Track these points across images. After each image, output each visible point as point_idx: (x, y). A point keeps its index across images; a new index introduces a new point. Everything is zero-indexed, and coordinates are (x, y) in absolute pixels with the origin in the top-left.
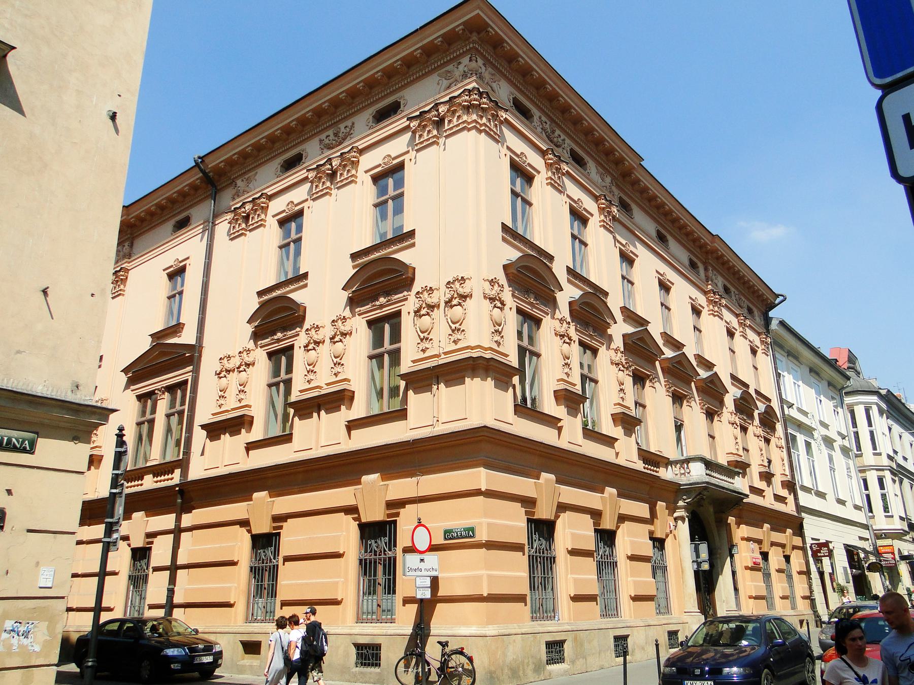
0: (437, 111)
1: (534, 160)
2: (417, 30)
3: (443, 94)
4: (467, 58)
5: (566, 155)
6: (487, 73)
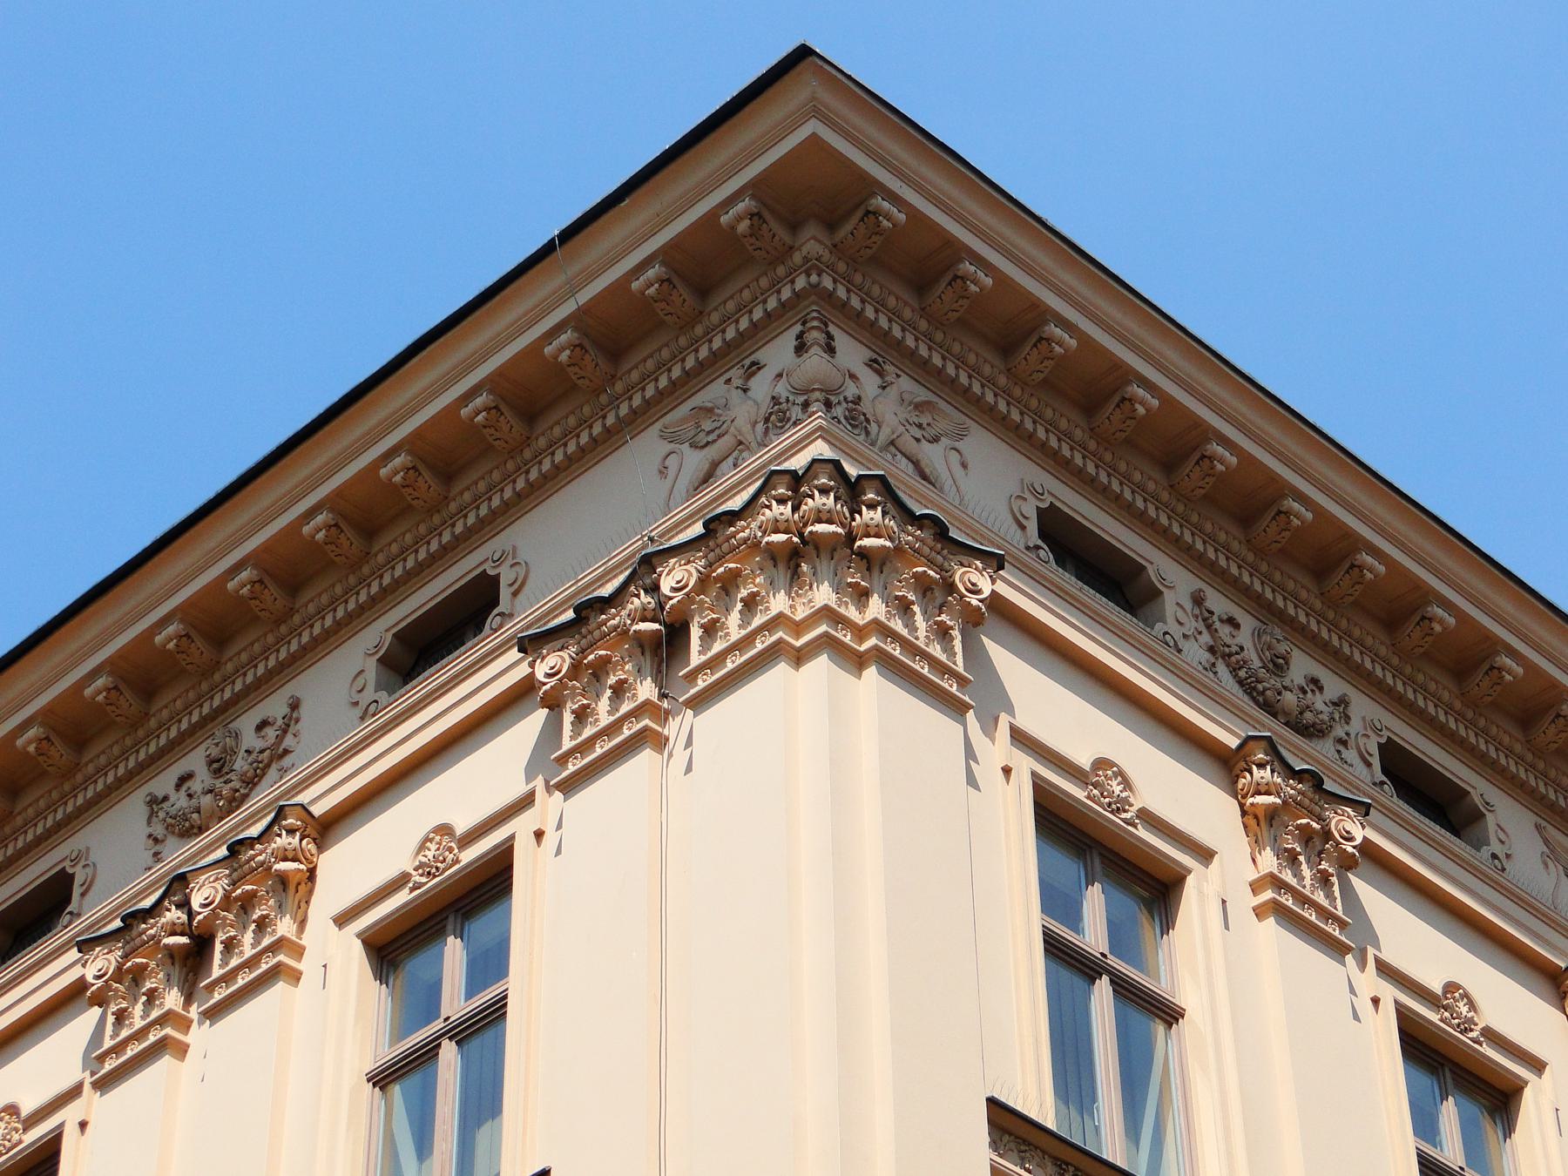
0: (654, 589)
1: (1172, 793)
2: (547, 250)
3: (680, 512)
4: (788, 340)
5: (1365, 775)
6: (888, 403)
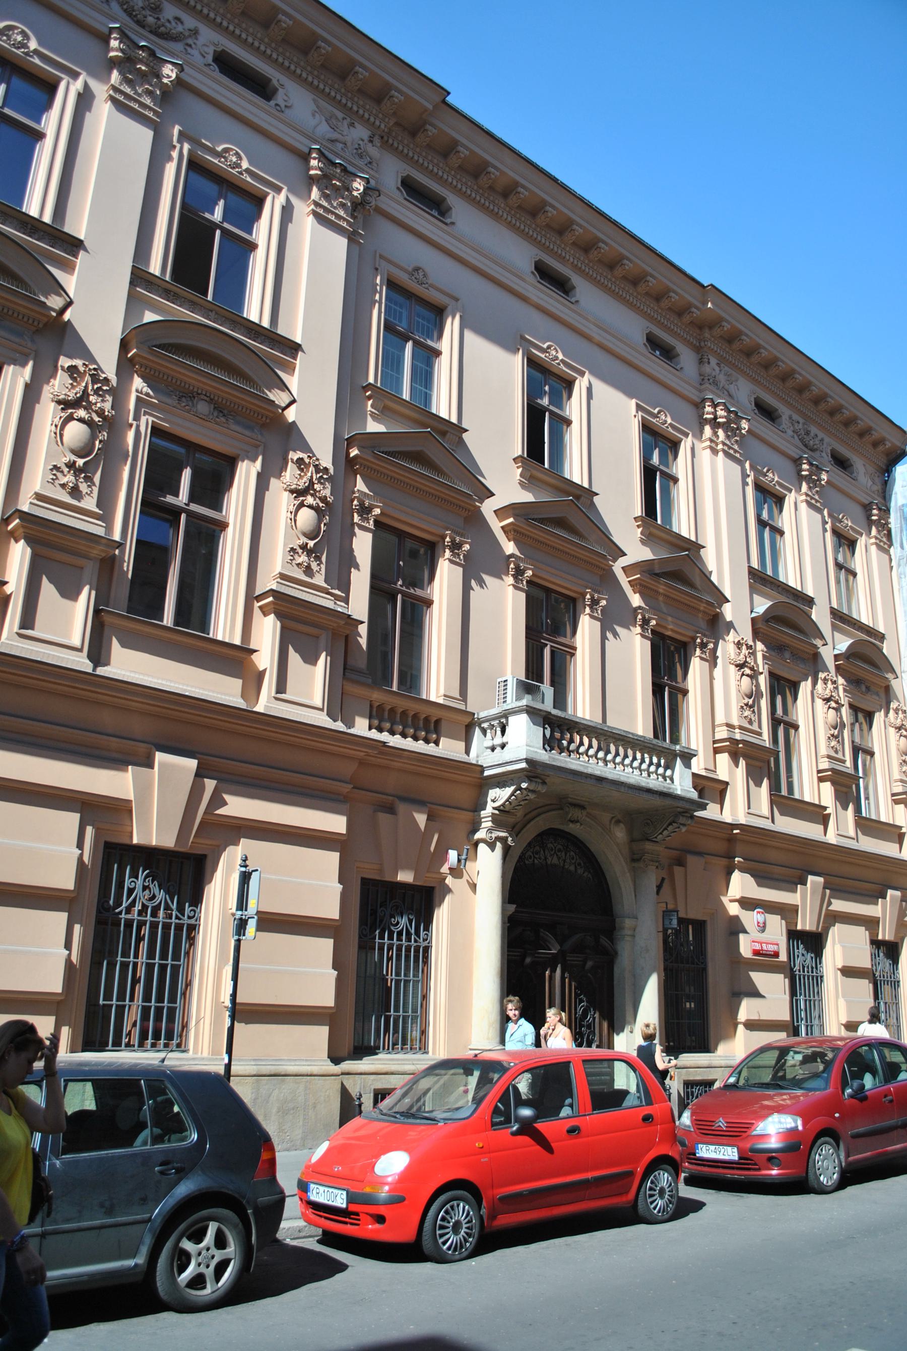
5: (826, 458)
